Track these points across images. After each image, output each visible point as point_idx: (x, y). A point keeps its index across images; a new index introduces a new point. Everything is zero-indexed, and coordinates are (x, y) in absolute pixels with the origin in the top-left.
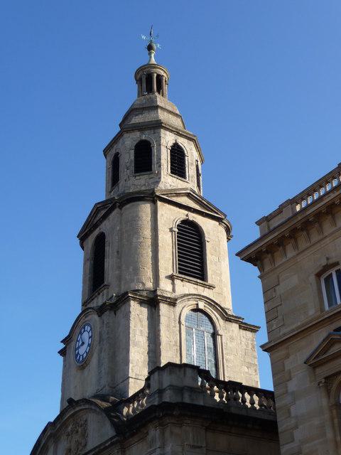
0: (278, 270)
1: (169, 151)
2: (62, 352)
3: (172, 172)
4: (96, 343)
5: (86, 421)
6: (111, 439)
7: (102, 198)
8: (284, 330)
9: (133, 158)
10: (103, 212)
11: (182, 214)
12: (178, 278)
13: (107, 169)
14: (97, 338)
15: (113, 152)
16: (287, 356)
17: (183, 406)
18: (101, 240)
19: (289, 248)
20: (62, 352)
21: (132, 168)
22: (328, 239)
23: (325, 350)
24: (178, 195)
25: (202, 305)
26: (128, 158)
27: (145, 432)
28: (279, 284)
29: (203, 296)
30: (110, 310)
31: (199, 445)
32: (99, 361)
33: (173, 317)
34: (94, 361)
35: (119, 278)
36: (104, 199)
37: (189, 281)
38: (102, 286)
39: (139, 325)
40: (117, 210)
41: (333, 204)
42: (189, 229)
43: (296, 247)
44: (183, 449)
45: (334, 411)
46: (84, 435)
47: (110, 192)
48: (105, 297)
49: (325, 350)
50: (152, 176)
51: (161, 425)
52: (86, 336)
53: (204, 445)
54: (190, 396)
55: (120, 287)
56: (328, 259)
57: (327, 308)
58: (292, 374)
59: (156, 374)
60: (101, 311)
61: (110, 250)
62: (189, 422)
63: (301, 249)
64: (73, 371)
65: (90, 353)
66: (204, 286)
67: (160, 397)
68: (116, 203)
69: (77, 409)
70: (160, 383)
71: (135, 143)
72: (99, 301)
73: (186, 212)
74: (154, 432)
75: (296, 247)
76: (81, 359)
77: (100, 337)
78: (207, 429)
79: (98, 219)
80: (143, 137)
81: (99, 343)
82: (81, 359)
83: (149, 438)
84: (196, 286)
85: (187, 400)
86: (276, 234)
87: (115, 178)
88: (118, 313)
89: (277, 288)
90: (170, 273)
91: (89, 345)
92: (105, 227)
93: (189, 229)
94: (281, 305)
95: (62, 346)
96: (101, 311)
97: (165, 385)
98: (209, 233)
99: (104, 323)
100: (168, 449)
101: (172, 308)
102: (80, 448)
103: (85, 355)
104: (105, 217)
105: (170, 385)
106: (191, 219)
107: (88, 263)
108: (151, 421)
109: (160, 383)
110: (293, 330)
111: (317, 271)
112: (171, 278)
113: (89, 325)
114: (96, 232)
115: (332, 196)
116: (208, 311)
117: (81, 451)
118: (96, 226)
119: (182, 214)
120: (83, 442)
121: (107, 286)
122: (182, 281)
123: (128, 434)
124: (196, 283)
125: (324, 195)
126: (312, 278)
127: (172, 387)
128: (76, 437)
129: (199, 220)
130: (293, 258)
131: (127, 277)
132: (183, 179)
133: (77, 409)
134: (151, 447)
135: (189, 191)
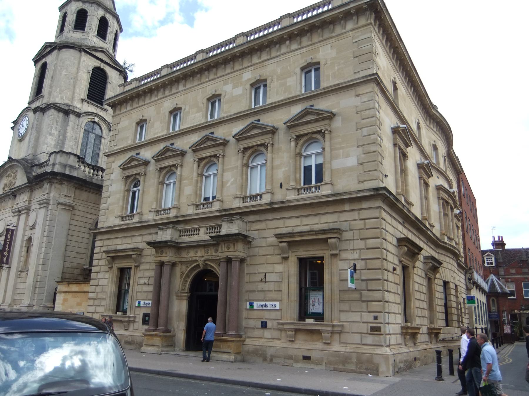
0: (121, 115)
1: (99, 21)
2: (13, 128)
3: (97, 35)
4: (30, 128)
5: (17, 171)
6: (25, 184)
7: (53, 40)
8: (116, 148)
9: (75, 18)
10: (49, 49)
11: (97, 63)
12: (86, 101)
13: (59, 21)
14: (31, 126)
15: (64, 10)
16: (113, 162)
17: (63, 175)
18: (44, 66)
19: (129, 105)
20: (13, 128)
21: (73, 26)
22: (146, 106)
23: (129, 163)
24: (97, 51)
25: (96, 119)
26: (71, 18)
27: (42, 184)
28: (119, 123)
29: (99, 115)
30: (40, 111)
31: (70, 195)
32: (30, 139)
33: (77, 123)
34: (27, 139)
35: (50, 93)
36: (54, 42)
37: (92, 104)
38: (40, 95)
39: (55, 123)
40: (56, 52)
41: (227, 58)
42: (100, 73)
43: (132, 105)
44: (60, 197)
45: (126, 193)
46: (15, 178)
47: (58, 37)
48: (40, 102)
49: (129, 163)
50: (84, 34)
51: (50, 182)
52: (25, 123)
53: (73, 196)
54: (70, 170)
55: (50, 99)
56: (143, 116)
57: (313, 89)
58: (114, 171)
59: (54, 155)
60: (35, 111)
61: (48, 74)
62: (66, 183)
63: (165, 95)
64: (16, 141)
65: (26, 134)
66: (102, 109)
67: (53, 167)
68: (57, 46)
69: (13, 164)
70: (55, 160)
71: (78, 9)
72: (37, 104)
73: (100, 62)
74: (46, 186)
75: (132, 105)
76: (20, 136)
77: (33, 126)
78: (76, 188)
79: (45, 52)
80: (83, 7)
81: (32, 129)
82: (20, 136)
83: (44, 187)
84: (96, 108)
85: (67, 172)
86: (123, 96)
87: (62, 29)
88: (45, 114)
89: (118, 125)
90: (82, 97)
91: (26, 129)
92: (49, 59)
93: (100, 73)
94: (118, 134)
95: (13, 125)
96: (35, 111)
97: (57, 161)
98: (112, 78)
99: (36, 118)
100: (52, 195)
101: (77, 119)
102: (12, 185)
103: (23, 134)
104: (49, 53)
105: (59, 163)
106: (102, 67)
107: (36, 78)
108: (45, 179)
109: (55, 160)
110: (119, 149)
111: (137, 121)
112: (83, 100)
113: (28, 117)
114: (43, 61)
115: (152, 84)
116: (100, 124)
117: (12, 186)
118: (44, 57)
119: (97, 63)
120: (13, 181)
121: (43, 97)
122: (88, 103)
123: (34, 183)
124: (97, 106)
125: (262, 37)
126: (134, 124)
127: (60, 163)
128: (10, 178)
129: (107, 69)
130: (129, 110)
131: (55, 94)
132: (104, 41)
133: (13, 164)
134: (43, 192)
135: (104, 50)
